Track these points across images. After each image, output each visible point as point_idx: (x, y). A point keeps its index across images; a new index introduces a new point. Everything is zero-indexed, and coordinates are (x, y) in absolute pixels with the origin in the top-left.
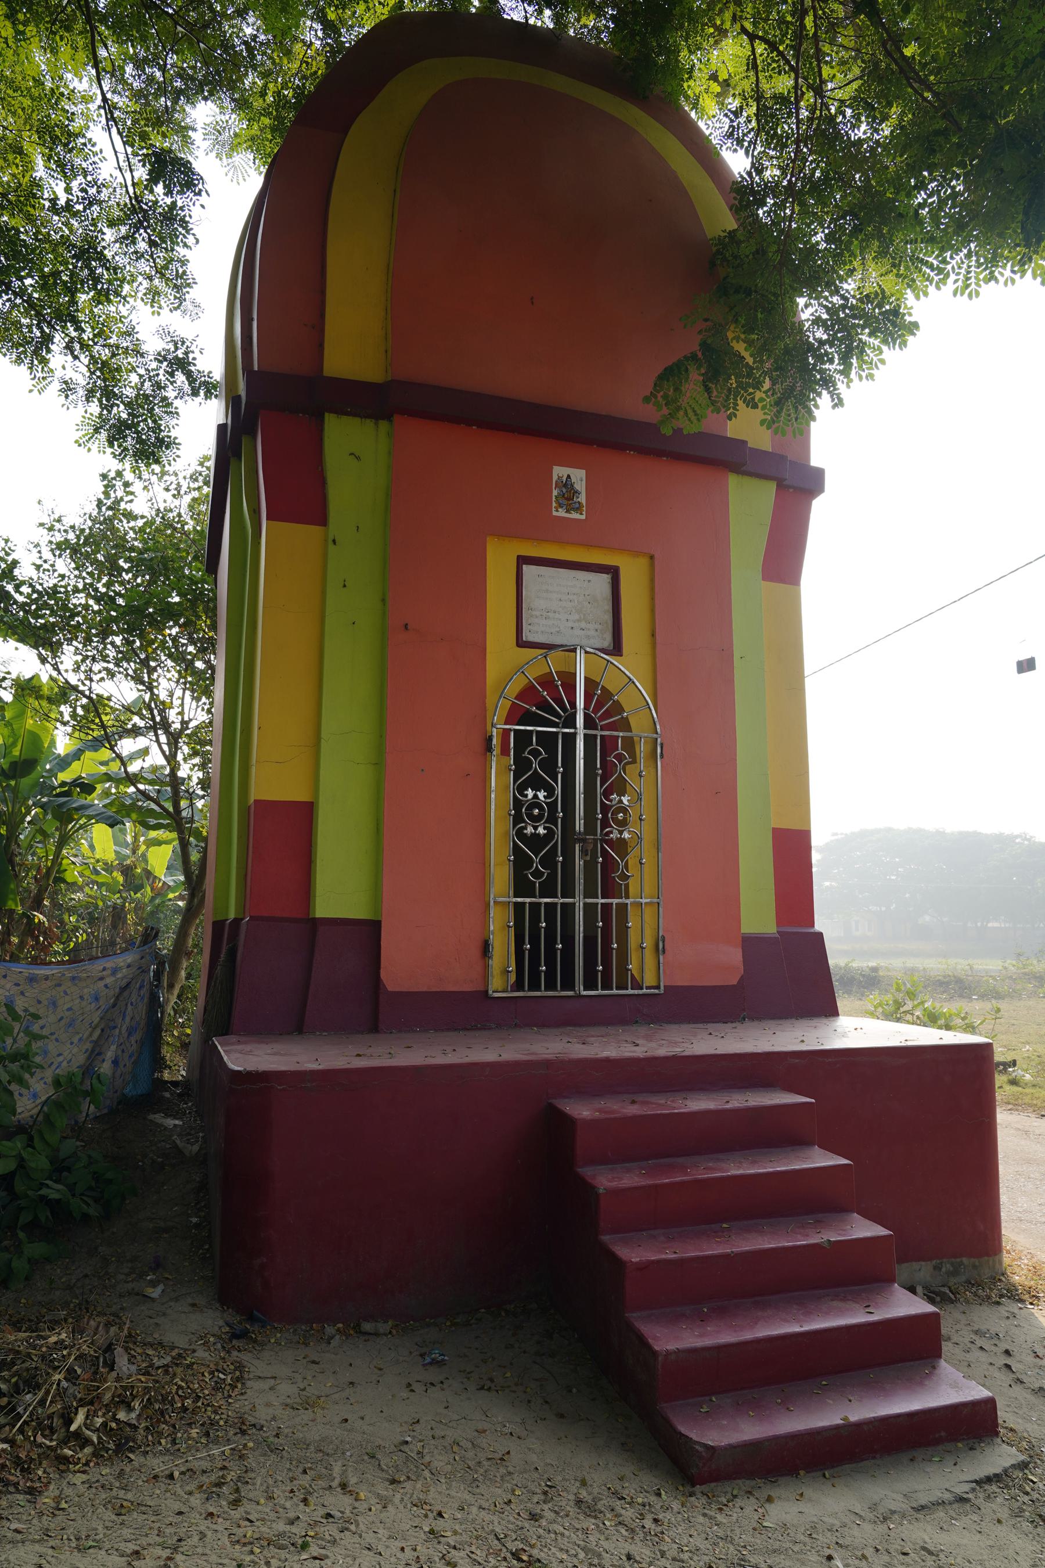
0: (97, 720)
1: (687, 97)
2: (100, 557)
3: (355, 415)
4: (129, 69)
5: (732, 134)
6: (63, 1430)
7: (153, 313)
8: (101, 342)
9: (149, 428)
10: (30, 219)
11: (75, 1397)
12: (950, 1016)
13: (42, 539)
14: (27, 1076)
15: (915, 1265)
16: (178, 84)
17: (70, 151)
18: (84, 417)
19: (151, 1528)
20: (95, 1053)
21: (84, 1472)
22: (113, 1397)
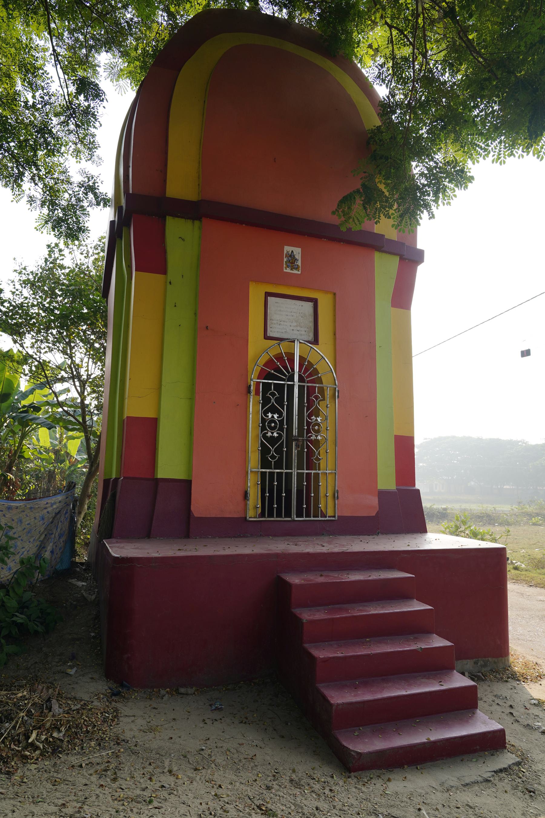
0: (43, 373)
1: (356, 57)
2: (46, 288)
3: (182, 217)
4: (66, 34)
5: (379, 76)
6: (25, 742)
7: (77, 162)
8: (50, 176)
9: (74, 222)
10: (13, 111)
11: (31, 725)
12: (484, 534)
13: (16, 278)
14: (6, 559)
15: (465, 662)
16: (91, 42)
17: (35, 77)
18: (40, 215)
19: (71, 792)
20: (42, 547)
21: (36, 763)
22: (51, 725)
